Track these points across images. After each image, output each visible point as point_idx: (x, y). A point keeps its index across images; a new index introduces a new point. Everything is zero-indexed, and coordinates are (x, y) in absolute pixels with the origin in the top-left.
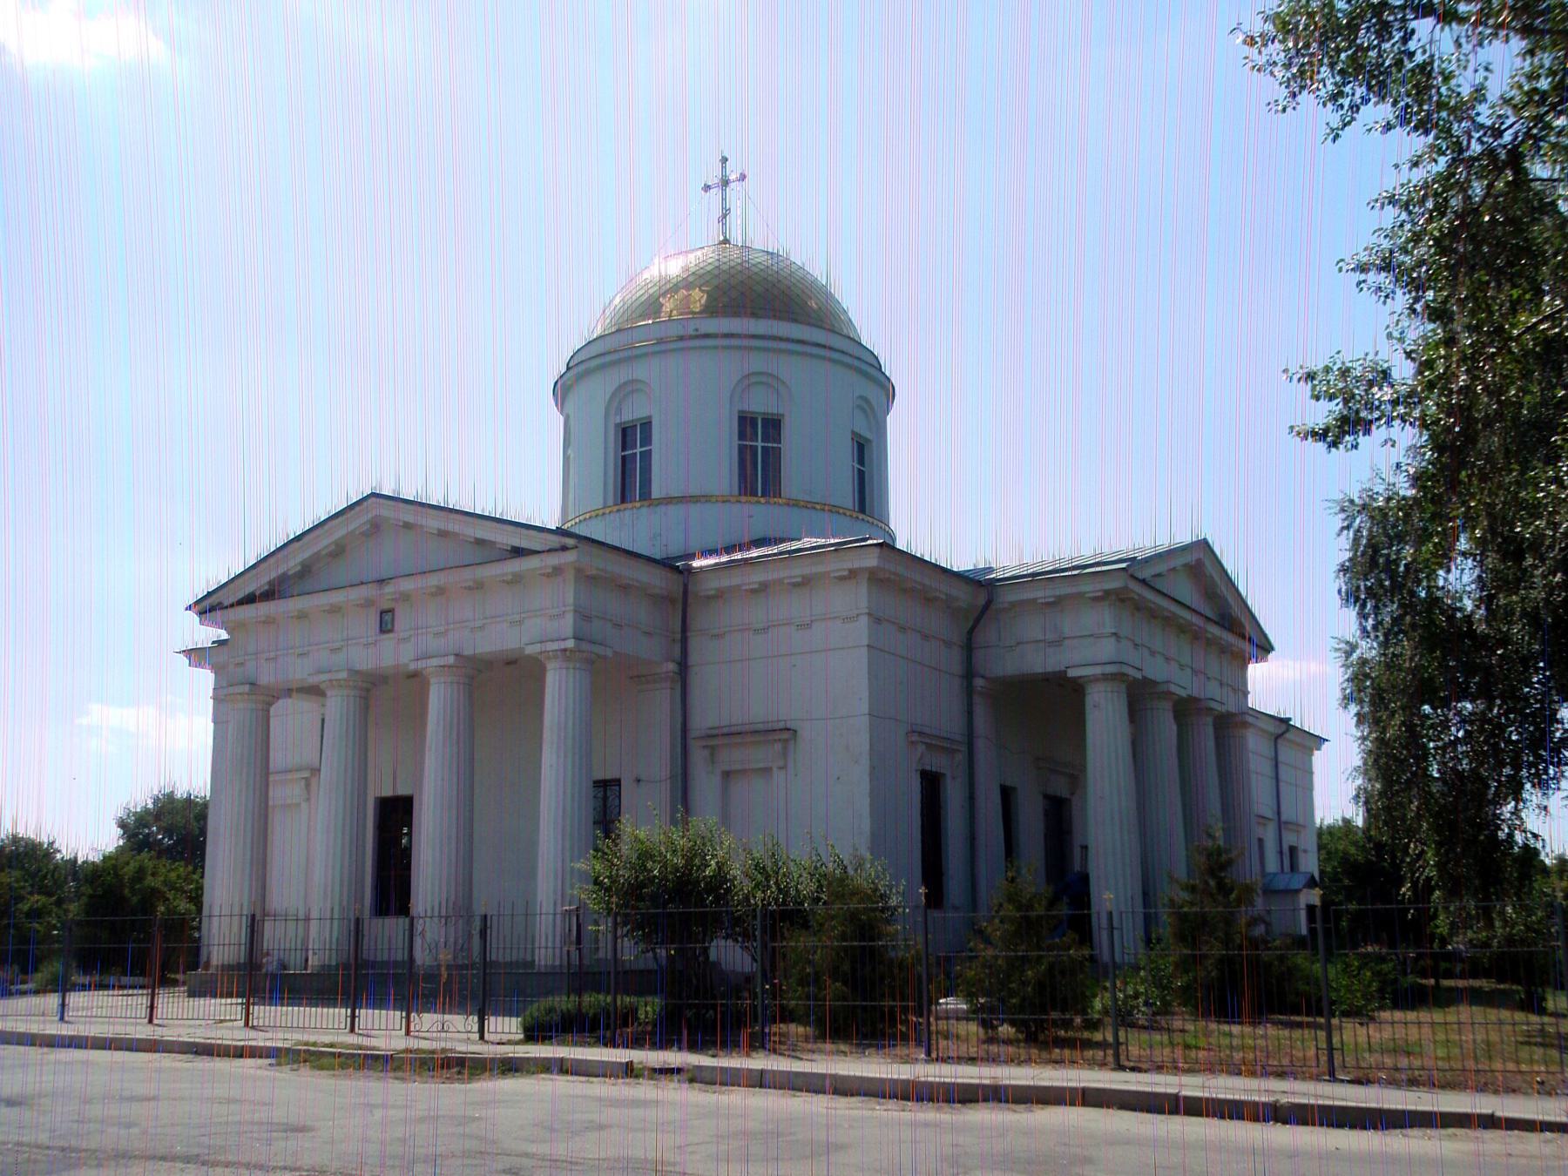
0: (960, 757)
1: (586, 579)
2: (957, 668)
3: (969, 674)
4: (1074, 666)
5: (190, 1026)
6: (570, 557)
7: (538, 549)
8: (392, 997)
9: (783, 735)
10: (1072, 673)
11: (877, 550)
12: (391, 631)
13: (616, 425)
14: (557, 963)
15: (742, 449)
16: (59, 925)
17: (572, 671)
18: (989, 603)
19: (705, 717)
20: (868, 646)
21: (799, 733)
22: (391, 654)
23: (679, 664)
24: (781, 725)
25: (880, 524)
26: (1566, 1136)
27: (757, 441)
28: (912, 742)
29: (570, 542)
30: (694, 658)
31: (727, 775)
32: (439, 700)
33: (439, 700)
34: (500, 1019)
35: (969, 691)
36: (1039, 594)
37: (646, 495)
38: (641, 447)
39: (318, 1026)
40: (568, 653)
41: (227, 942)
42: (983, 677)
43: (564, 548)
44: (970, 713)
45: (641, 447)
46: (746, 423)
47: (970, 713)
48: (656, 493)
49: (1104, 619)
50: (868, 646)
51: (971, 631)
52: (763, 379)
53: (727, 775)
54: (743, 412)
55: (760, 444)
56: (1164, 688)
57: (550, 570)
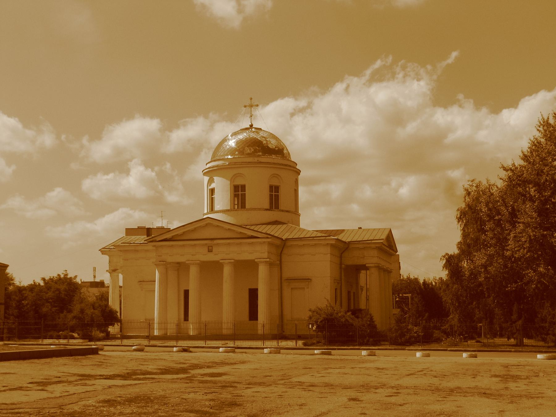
1: (270, 244)
3: (341, 264)
6: (269, 240)
7: (260, 237)
9: (308, 280)
10: (367, 265)
11: (335, 240)
12: (212, 251)
13: (233, 185)
14: (232, 332)
15: (271, 196)
16: (431, 323)
18: (348, 247)
19: (286, 275)
20: (330, 261)
22: (211, 257)
25: (296, 213)
27: (274, 194)
29: (270, 236)
30: (283, 260)
31: (292, 288)
32: (227, 270)
33: (227, 270)
34: (268, 342)
35: (341, 268)
36: (361, 246)
37: (245, 207)
41: (136, 329)
42: (344, 265)
43: (268, 238)
44: (341, 273)
46: (271, 187)
47: (341, 273)
48: (247, 206)
49: (375, 253)
50: (330, 261)
51: (342, 254)
52: (276, 175)
54: (271, 185)
55: (274, 194)
57: (227, 229)
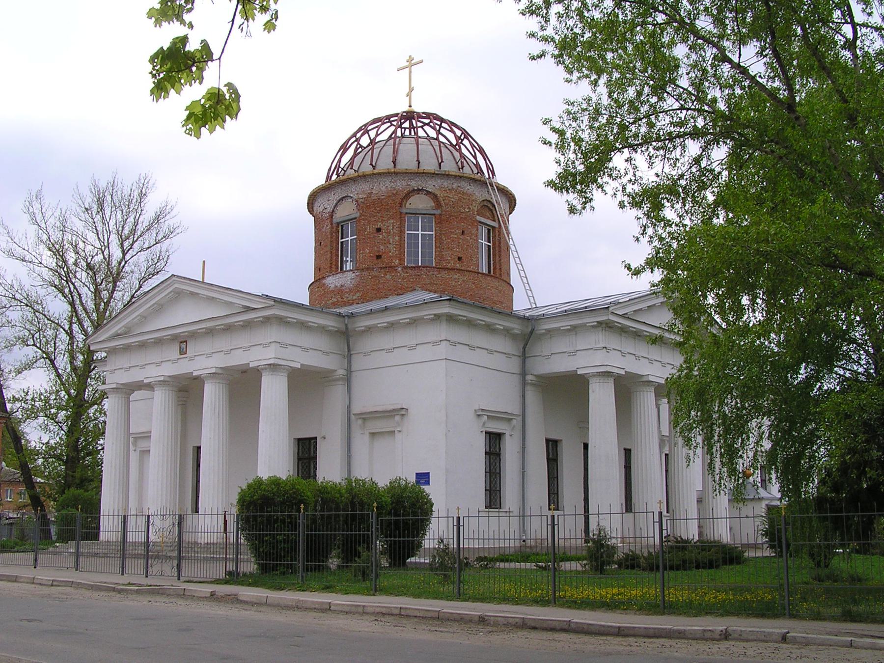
0: (516, 422)
2: (517, 369)
3: (523, 374)
4: (349, 407)
5: (653, 445)
8: (302, 532)
9: (401, 412)
17: (117, 399)
21: (409, 410)
23: (347, 370)
24: (400, 407)
26: (883, 625)
28: (479, 415)
35: (524, 383)
38: (348, 240)
39: (130, 573)
40: (272, 366)
45: (348, 240)
53: (373, 435)
56: (644, 379)
